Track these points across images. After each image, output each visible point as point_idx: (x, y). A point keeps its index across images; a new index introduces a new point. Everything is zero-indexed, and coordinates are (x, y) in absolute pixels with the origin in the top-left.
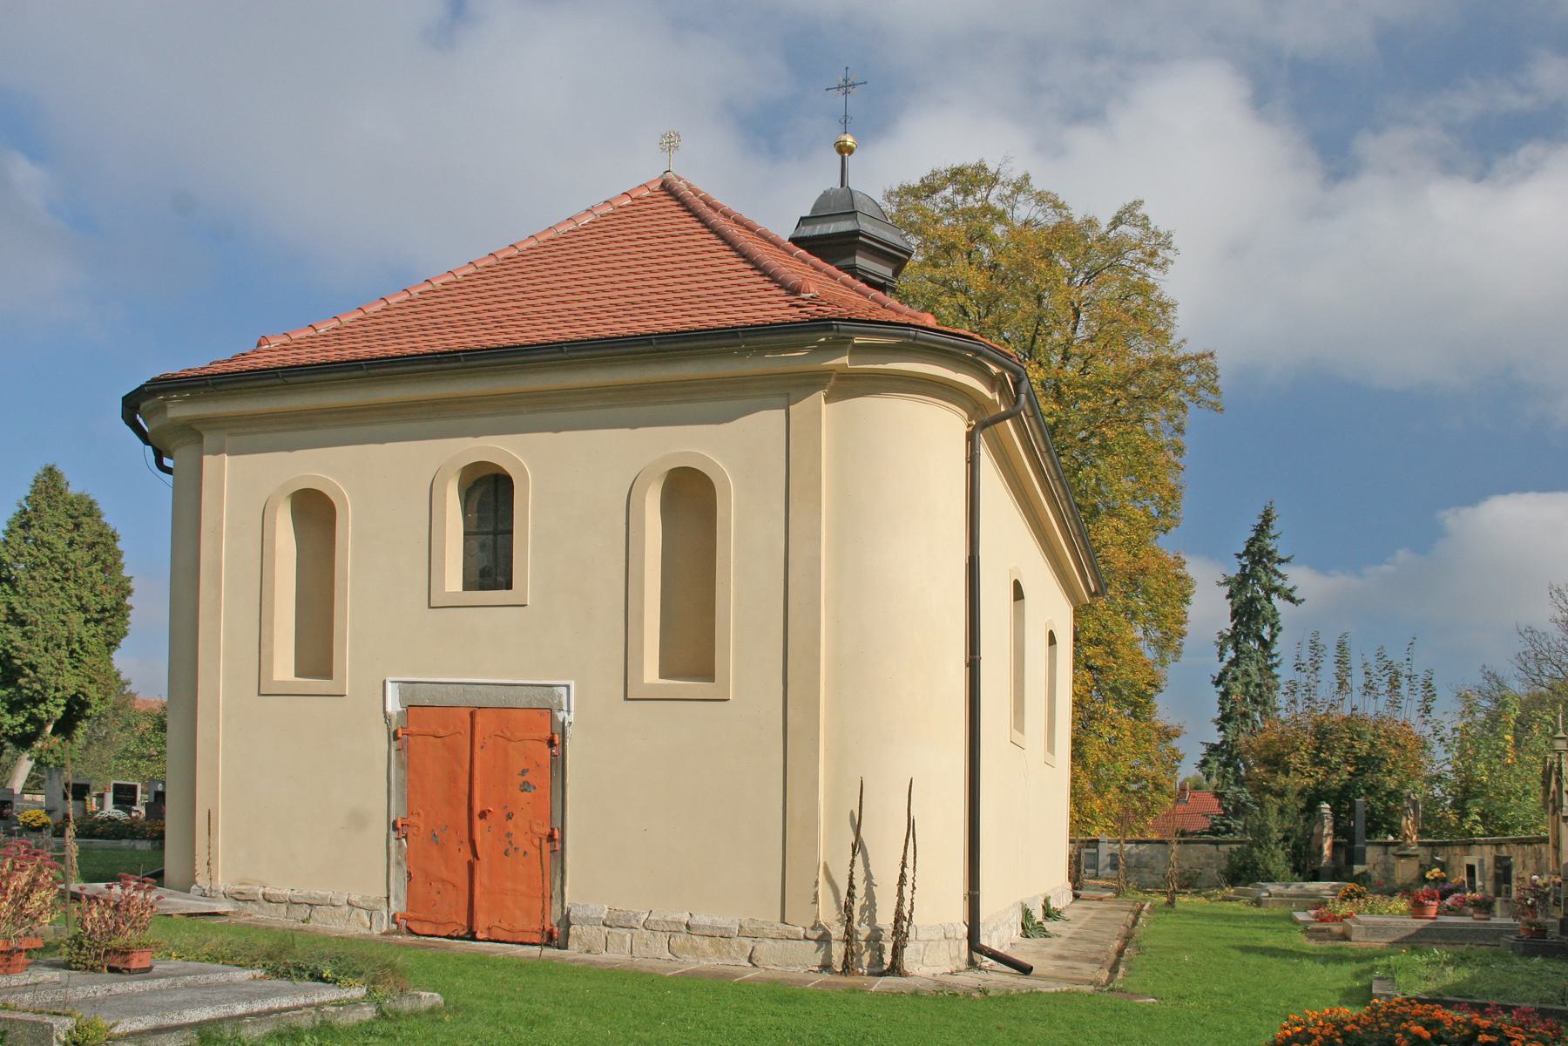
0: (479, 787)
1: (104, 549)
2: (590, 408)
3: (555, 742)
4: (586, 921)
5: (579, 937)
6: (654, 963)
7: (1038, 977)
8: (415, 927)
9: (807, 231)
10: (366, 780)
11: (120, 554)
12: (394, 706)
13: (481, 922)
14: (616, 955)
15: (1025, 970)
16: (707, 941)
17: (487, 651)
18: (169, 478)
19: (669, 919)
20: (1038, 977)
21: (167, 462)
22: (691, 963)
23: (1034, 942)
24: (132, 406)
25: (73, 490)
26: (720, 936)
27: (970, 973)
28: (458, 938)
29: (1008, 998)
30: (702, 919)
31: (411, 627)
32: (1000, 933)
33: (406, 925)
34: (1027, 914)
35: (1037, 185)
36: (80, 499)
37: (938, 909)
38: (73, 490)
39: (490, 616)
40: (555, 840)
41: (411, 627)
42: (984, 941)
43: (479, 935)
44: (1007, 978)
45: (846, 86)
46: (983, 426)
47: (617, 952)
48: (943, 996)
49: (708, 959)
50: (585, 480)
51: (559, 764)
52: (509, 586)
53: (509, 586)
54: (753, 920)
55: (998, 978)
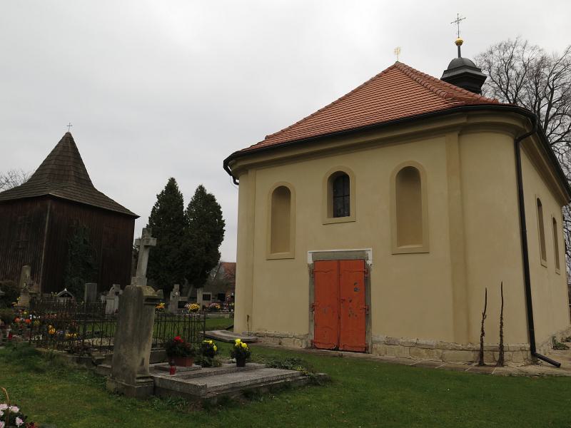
0: (341, 289)
1: (217, 210)
2: (310, 294)
3: (366, 271)
4: (379, 342)
5: (376, 349)
6: (405, 360)
7: (564, 369)
8: (317, 345)
9: (446, 76)
10: (300, 293)
11: (221, 213)
12: (310, 261)
13: (342, 343)
14: (390, 357)
15: (558, 366)
16: (424, 351)
17: (341, 239)
18: (238, 186)
19: (409, 341)
20: (564, 369)
21: (237, 181)
22: (418, 360)
23: (558, 352)
24: (227, 163)
25: (208, 192)
26: (429, 348)
27: (533, 366)
28: (333, 350)
29: (552, 377)
30: (422, 341)
31: (316, 233)
32: (543, 348)
33: (313, 345)
34: (554, 341)
35: (531, 44)
36: (209, 195)
37: (516, 338)
38: (208, 192)
39: (342, 227)
40: (367, 310)
41: (316, 233)
42: (538, 352)
43: (340, 349)
44: (549, 368)
45: (458, 21)
46: (521, 139)
47: (391, 355)
48: (521, 379)
49: (425, 359)
50: (373, 174)
51: (367, 280)
52: (349, 215)
53: (349, 215)
54: (441, 342)
55: (545, 369)
